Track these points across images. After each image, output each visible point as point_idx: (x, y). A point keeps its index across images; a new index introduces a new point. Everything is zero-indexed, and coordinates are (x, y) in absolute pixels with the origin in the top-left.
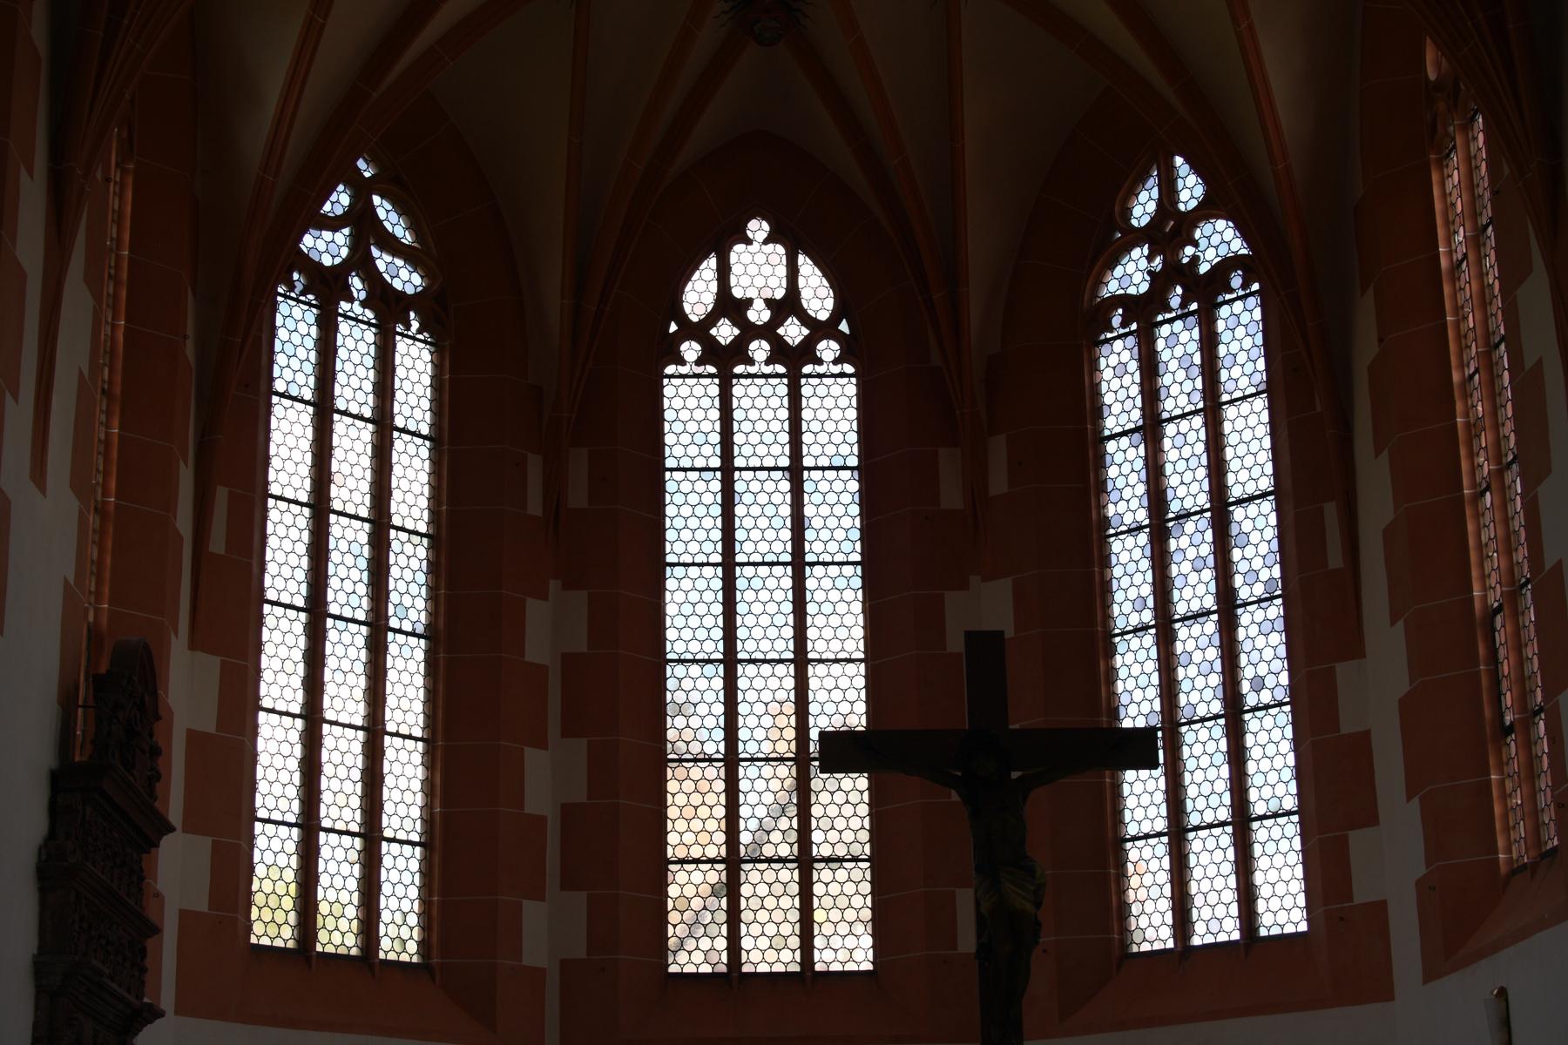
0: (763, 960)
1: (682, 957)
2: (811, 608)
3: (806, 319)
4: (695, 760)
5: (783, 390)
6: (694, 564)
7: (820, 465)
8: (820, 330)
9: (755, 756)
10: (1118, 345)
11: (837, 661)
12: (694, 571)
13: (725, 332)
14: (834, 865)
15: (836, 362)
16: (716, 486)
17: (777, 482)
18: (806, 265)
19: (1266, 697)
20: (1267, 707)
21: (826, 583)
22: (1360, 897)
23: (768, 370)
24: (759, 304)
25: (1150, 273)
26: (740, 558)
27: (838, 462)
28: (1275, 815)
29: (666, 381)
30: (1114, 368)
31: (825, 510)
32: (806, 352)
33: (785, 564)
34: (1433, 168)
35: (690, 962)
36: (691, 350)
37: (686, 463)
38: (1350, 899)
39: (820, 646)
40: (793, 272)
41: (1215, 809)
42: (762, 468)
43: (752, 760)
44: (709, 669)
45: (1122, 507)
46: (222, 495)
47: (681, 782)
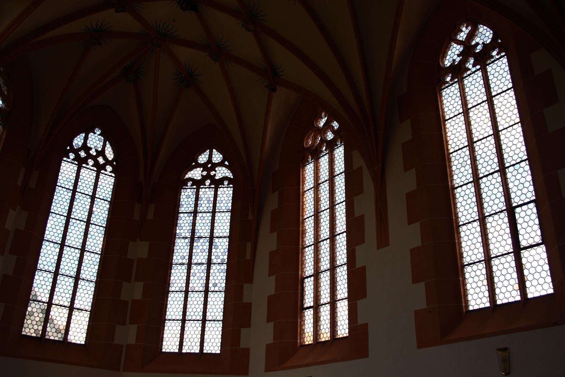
0: (53, 335)
1: (27, 330)
2: (89, 236)
3: (105, 158)
4: (45, 271)
5: (95, 175)
6: (58, 214)
7: (100, 198)
8: (107, 162)
9: (64, 274)
10: (189, 190)
11: (93, 253)
12: (58, 216)
14: (80, 311)
15: (110, 172)
16: (70, 194)
17: (87, 199)
18: (108, 145)
19: (217, 289)
20: (216, 292)
21: (221, 218)
22: (242, 346)
23: (92, 168)
24: (93, 150)
25: (201, 175)
26: (72, 216)
27: (105, 198)
28: (214, 321)
29: (63, 161)
30: (186, 196)
31: (99, 210)
32: (103, 167)
33: (84, 222)
34: (301, 167)
35: (29, 332)
36: (72, 156)
37: (63, 185)
38: (239, 346)
39: (89, 247)
40: (104, 146)
41: (196, 316)
42: (84, 194)
43: (63, 275)
44: (56, 245)
45: (182, 231)
47: (40, 276)
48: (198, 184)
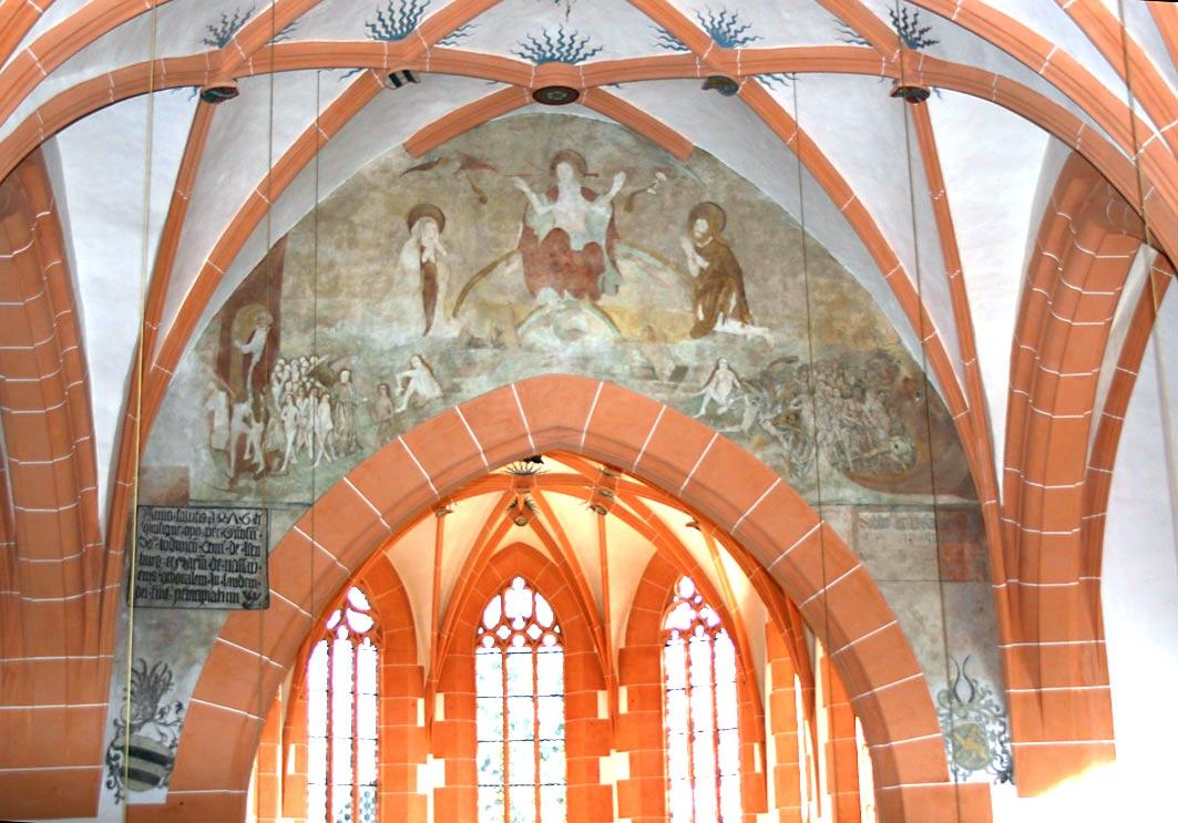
13: (504, 633)
46: (292, 748)
48: (686, 634)
